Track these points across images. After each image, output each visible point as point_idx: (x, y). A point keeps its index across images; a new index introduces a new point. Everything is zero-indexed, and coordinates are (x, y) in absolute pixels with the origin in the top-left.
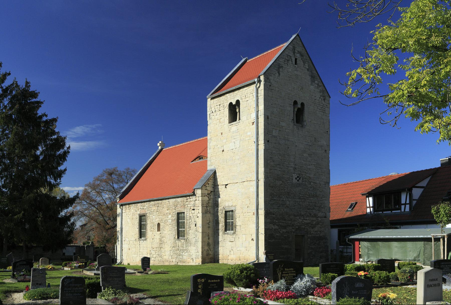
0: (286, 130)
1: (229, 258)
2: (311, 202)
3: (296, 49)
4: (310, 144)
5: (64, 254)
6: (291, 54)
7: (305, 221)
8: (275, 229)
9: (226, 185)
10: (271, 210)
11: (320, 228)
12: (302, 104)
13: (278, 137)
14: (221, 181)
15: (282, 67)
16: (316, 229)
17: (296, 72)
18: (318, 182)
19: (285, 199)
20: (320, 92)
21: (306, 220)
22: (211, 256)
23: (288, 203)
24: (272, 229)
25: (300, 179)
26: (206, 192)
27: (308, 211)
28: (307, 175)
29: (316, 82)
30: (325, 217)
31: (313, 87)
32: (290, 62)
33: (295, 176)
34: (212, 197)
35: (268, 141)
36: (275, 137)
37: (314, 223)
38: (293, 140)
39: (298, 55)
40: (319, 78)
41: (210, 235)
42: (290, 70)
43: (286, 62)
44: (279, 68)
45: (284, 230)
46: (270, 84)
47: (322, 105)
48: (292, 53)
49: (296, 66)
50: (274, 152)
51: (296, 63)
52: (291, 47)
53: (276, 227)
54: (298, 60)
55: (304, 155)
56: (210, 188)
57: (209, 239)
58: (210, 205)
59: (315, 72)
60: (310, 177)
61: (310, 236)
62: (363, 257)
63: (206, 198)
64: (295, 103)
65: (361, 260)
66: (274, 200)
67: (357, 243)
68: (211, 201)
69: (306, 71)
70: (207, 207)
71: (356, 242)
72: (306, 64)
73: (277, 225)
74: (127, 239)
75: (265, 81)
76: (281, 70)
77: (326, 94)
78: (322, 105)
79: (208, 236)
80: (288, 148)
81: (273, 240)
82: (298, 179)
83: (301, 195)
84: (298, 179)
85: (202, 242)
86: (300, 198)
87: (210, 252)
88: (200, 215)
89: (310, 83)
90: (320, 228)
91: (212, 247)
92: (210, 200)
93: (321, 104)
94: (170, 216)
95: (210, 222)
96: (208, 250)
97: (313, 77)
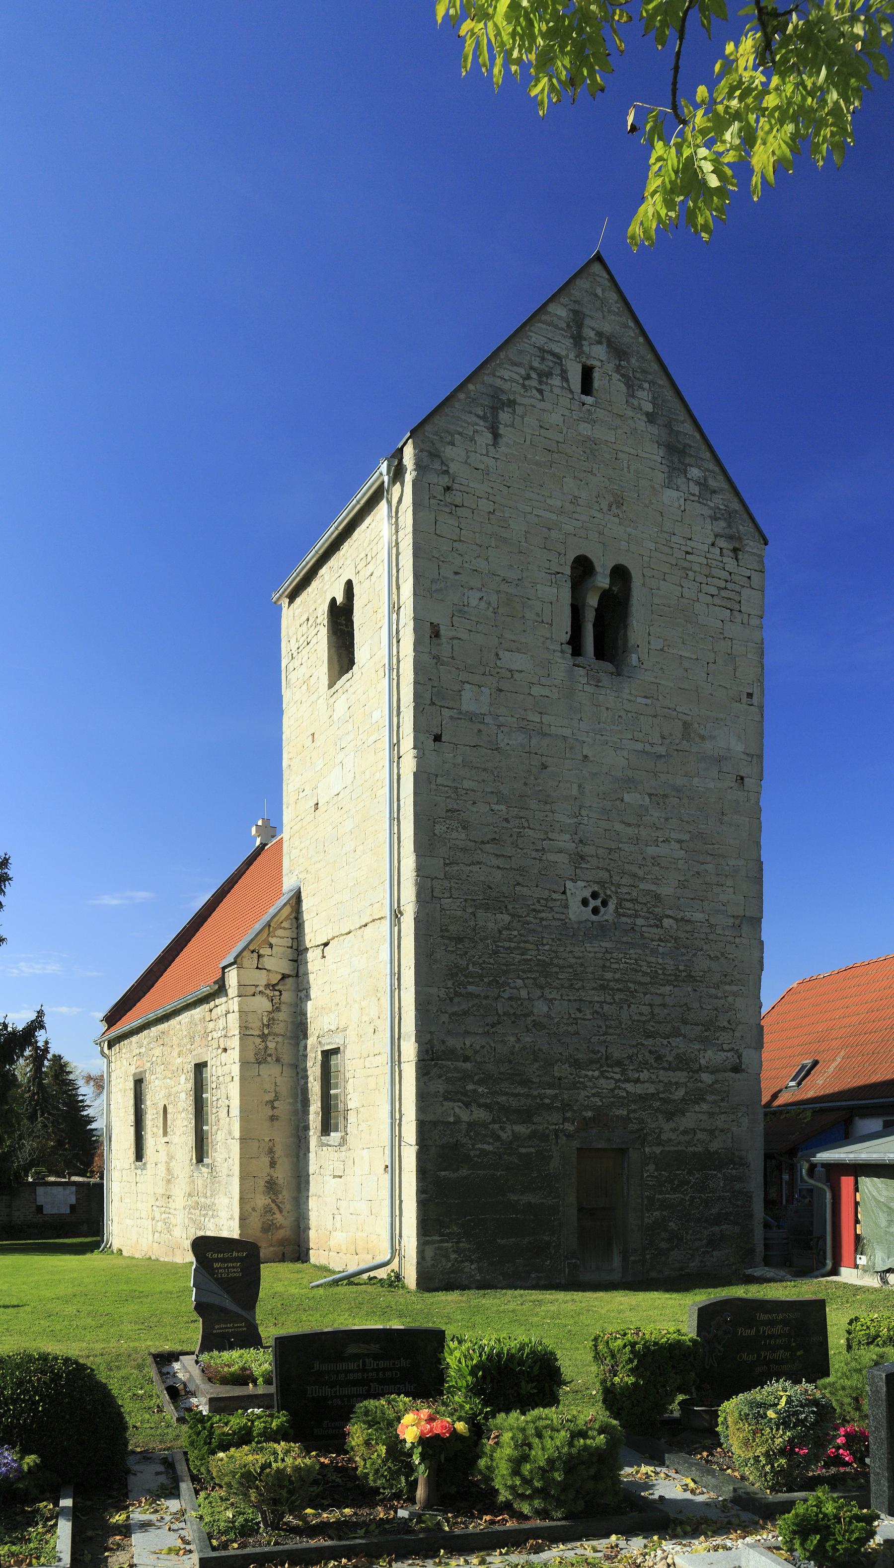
0: (535, 690)
1: (332, 1243)
2: (664, 1005)
3: (588, 322)
4: (662, 750)
5: (40, 1209)
6: (563, 346)
7: (630, 1087)
8: (471, 1125)
9: (326, 944)
10: (453, 1042)
11: (711, 1115)
12: (620, 574)
13: (488, 720)
14: (314, 932)
15: (512, 403)
16: (688, 1121)
17: (585, 429)
18: (699, 916)
19: (524, 993)
20: (714, 518)
21: (637, 1081)
22: (281, 1234)
23: (541, 1008)
24: (458, 1121)
25: (604, 903)
26: (262, 979)
27: (649, 1042)
28: (642, 886)
29: (694, 472)
30: (736, 1069)
31: (675, 494)
32: (556, 381)
33: (578, 891)
34: (287, 996)
35: (437, 738)
36: (471, 717)
37: (681, 1093)
38: (567, 732)
39: (598, 353)
40: (708, 455)
41: (279, 1152)
42: (555, 418)
43: (534, 383)
44: (495, 409)
45: (521, 1129)
46: (445, 481)
47: (725, 575)
48: (569, 342)
49: (589, 400)
50: (467, 784)
51: (587, 387)
52: (562, 312)
53: (480, 1114)
54: (596, 375)
55: (627, 797)
56: (277, 962)
57: (273, 1164)
58: (279, 1028)
59: (687, 428)
60: (657, 898)
61: (658, 1150)
62: (868, 1251)
63: (262, 1004)
64: (583, 568)
65: (862, 1260)
66: (471, 995)
67: (847, 1182)
68: (281, 1016)
69: (641, 424)
70: (263, 1037)
71: (844, 1179)
72: (640, 394)
73: (487, 1106)
74: (118, 1167)
75: (419, 466)
76: (504, 416)
77: (745, 528)
78: (725, 575)
79: (271, 1151)
80: (544, 767)
81: (464, 1172)
82: (593, 903)
83: (609, 975)
84: (593, 903)
85: (242, 1179)
86: (603, 988)
87: (279, 1218)
88: (236, 1070)
89: (660, 477)
90: (711, 1115)
91: (286, 1196)
92: (278, 1009)
93: (715, 572)
94: (183, 1078)
95: (277, 1098)
96: (268, 1211)
97: (677, 454)
